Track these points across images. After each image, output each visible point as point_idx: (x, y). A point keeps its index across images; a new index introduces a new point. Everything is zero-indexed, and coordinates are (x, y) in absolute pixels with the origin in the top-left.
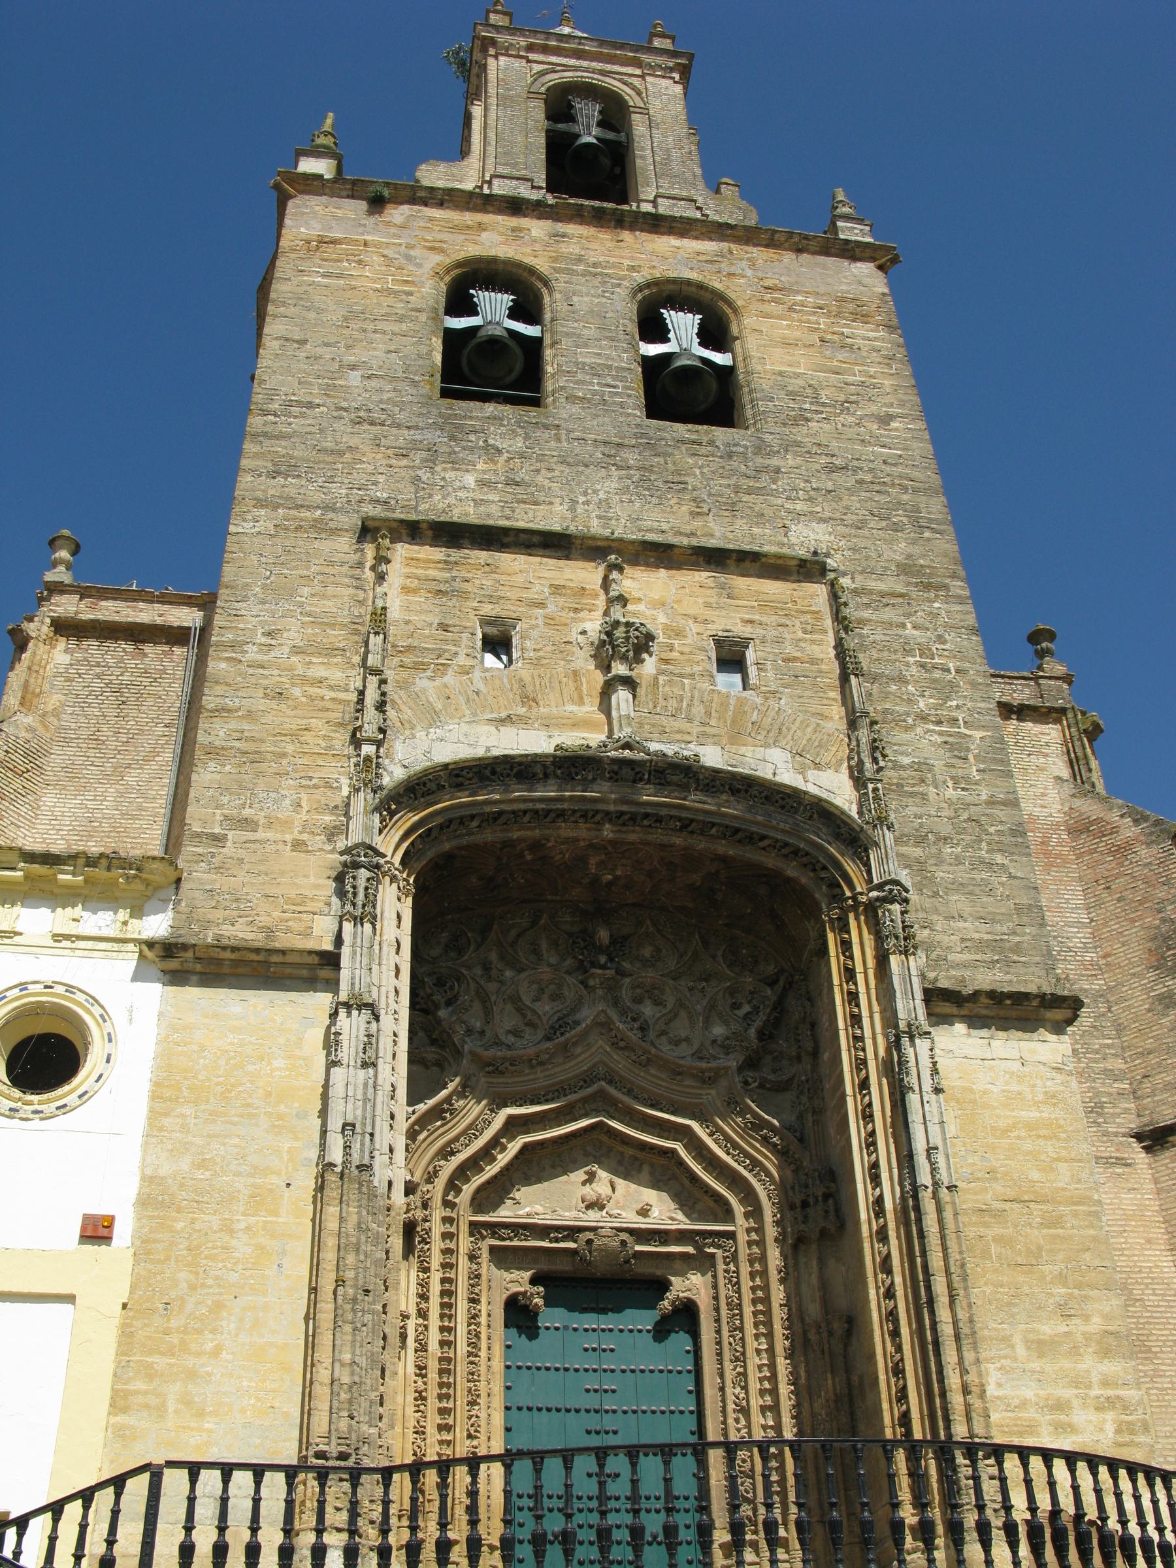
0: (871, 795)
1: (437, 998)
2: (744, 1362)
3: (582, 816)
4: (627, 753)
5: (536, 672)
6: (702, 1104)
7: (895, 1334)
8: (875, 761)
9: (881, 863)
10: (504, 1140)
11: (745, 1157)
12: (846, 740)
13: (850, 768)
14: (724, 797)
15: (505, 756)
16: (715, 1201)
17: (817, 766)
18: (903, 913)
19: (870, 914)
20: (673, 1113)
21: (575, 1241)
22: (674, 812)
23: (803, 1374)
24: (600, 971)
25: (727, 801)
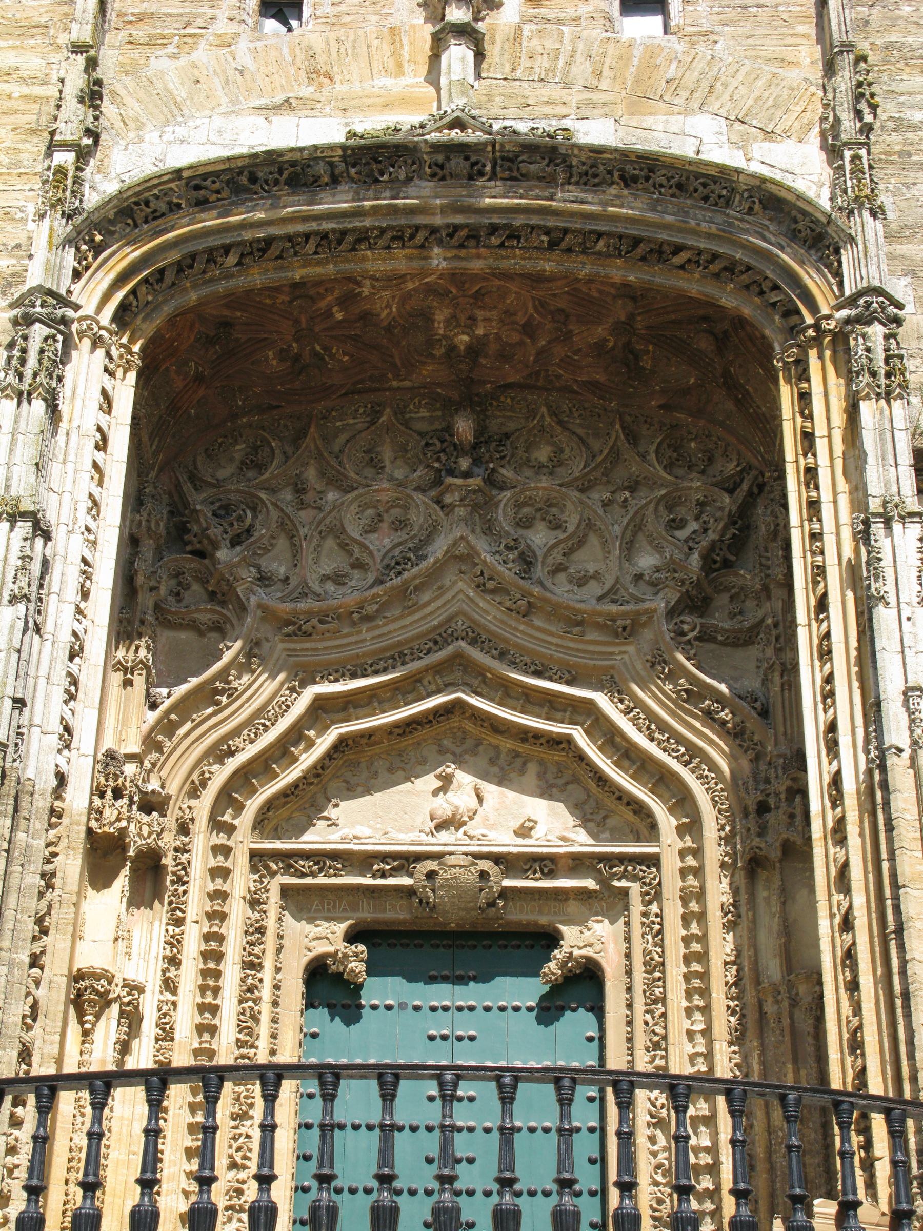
0: (848, 167)
1: (215, 531)
2: (666, 1050)
3: (394, 238)
4: (455, 135)
5: (333, 36)
6: (613, 667)
7: (853, 986)
8: (859, 114)
9: (857, 266)
10: (312, 733)
11: (678, 743)
12: (821, 93)
13: (823, 134)
14: (613, 190)
15: (269, 153)
16: (635, 812)
17: (768, 135)
18: (887, 337)
19: (841, 348)
20: (568, 683)
21: (411, 875)
22: (535, 220)
23: (756, 1067)
24: (459, 481)
25: (618, 197)
